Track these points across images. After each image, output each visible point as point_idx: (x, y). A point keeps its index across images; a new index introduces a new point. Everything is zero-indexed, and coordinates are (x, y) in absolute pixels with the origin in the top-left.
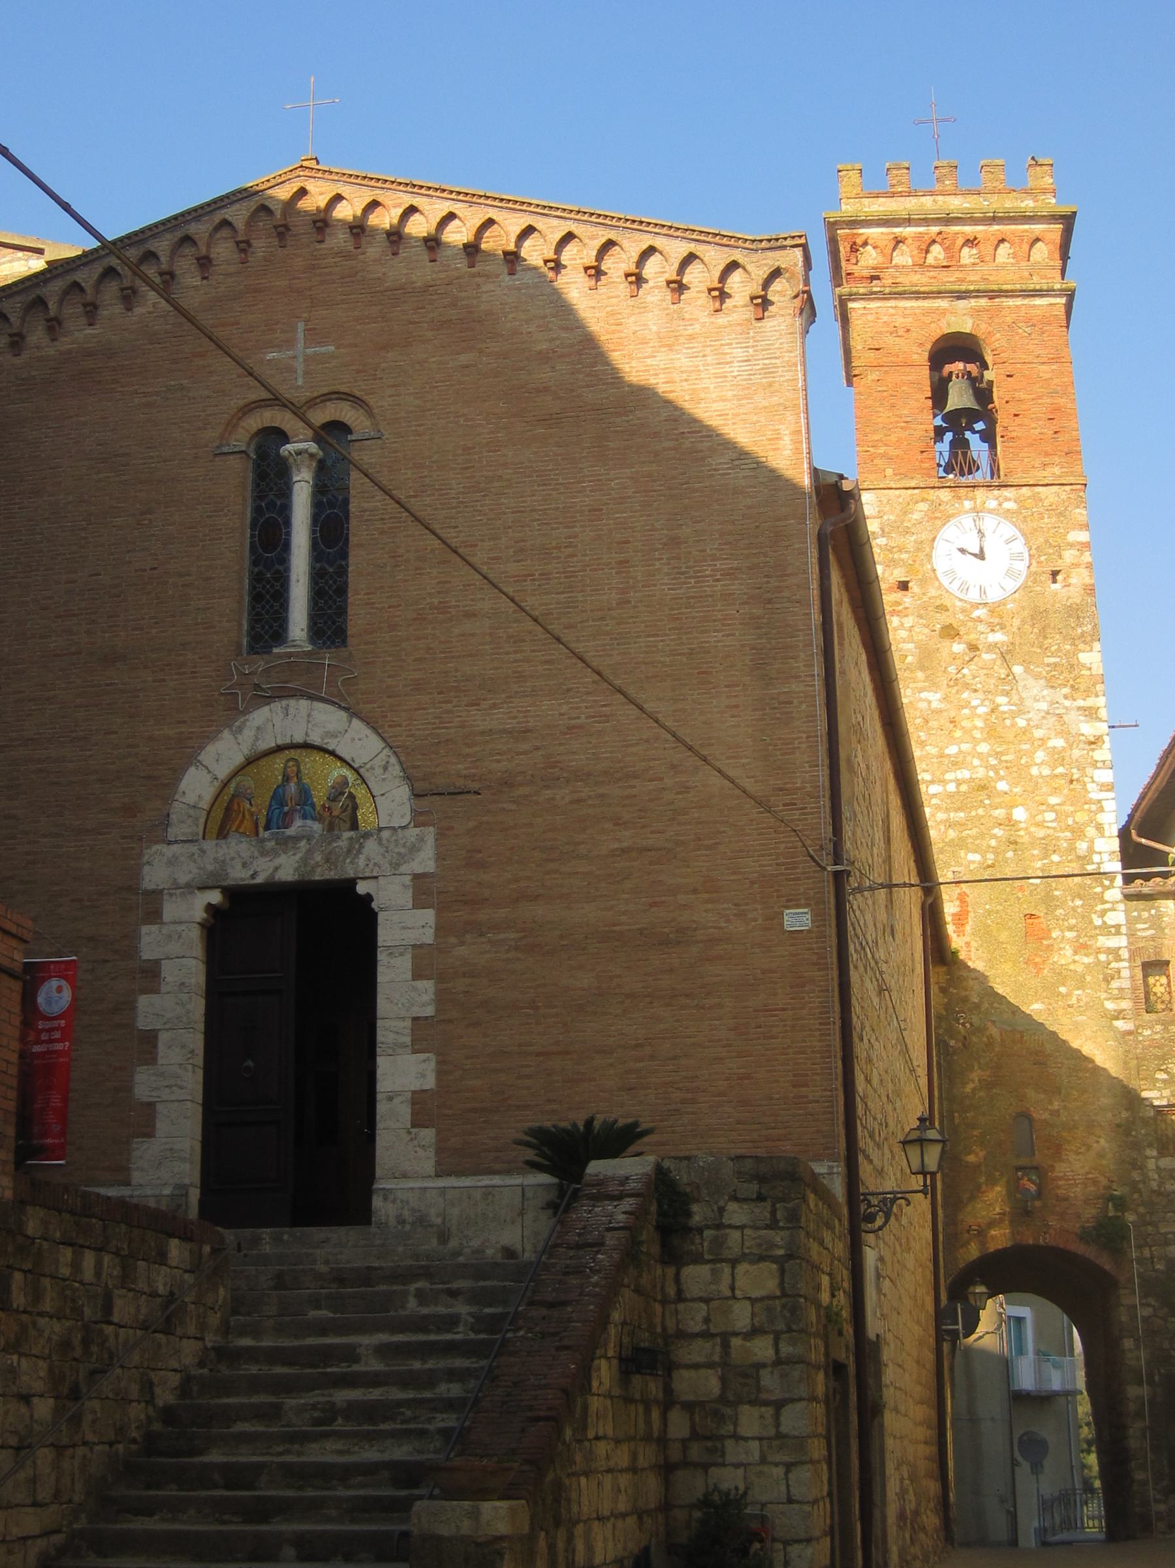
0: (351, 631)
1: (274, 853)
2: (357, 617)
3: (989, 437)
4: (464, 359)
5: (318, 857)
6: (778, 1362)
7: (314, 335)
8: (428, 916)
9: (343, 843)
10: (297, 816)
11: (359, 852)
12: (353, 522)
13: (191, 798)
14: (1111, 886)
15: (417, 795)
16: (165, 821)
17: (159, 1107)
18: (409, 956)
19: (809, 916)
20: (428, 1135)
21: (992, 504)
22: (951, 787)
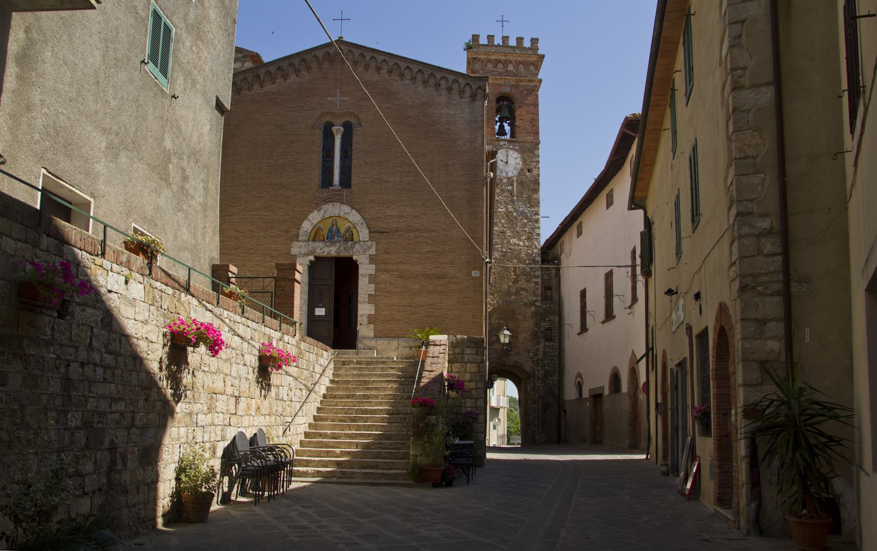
0: (353, 184)
1: (329, 246)
2: (355, 180)
4: (387, 105)
6: (477, 388)
8: (373, 266)
12: (353, 152)
13: (305, 229)
15: (370, 232)
16: (297, 236)
20: (372, 326)
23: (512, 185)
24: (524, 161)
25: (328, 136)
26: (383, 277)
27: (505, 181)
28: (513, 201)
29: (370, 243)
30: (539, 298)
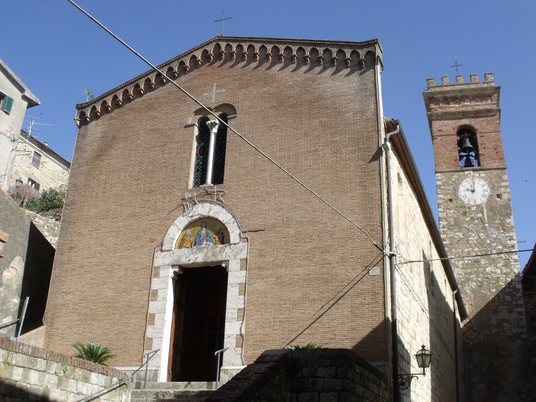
3: (477, 157)
5: (210, 254)
7: (219, 87)
9: (218, 249)
10: (204, 240)
11: (223, 252)
14: (519, 292)
17: (154, 339)
18: (238, 287)
19: (379, 270)
21: (477, 175)
22: (467, 261)
23: (482, 212)
24: (492, 188)
25: (204, 132)
26: (259, 285)
27: (474, 209)
28: (484, 228)
29: (241, 244)
30: (525, 330)
